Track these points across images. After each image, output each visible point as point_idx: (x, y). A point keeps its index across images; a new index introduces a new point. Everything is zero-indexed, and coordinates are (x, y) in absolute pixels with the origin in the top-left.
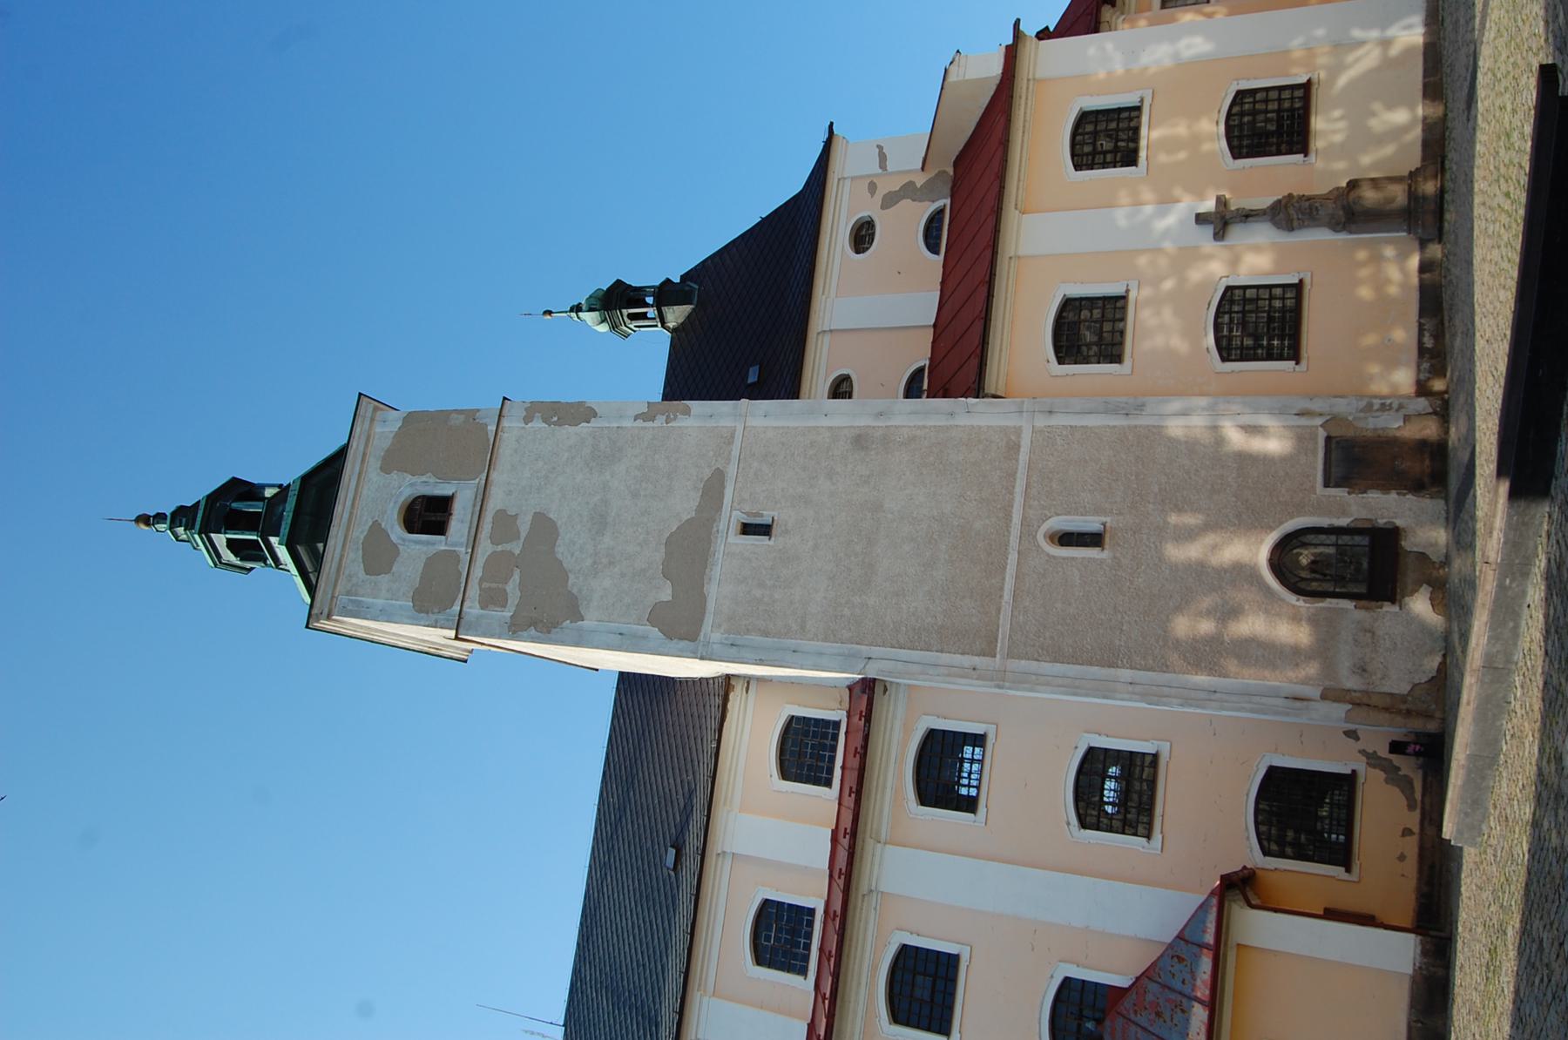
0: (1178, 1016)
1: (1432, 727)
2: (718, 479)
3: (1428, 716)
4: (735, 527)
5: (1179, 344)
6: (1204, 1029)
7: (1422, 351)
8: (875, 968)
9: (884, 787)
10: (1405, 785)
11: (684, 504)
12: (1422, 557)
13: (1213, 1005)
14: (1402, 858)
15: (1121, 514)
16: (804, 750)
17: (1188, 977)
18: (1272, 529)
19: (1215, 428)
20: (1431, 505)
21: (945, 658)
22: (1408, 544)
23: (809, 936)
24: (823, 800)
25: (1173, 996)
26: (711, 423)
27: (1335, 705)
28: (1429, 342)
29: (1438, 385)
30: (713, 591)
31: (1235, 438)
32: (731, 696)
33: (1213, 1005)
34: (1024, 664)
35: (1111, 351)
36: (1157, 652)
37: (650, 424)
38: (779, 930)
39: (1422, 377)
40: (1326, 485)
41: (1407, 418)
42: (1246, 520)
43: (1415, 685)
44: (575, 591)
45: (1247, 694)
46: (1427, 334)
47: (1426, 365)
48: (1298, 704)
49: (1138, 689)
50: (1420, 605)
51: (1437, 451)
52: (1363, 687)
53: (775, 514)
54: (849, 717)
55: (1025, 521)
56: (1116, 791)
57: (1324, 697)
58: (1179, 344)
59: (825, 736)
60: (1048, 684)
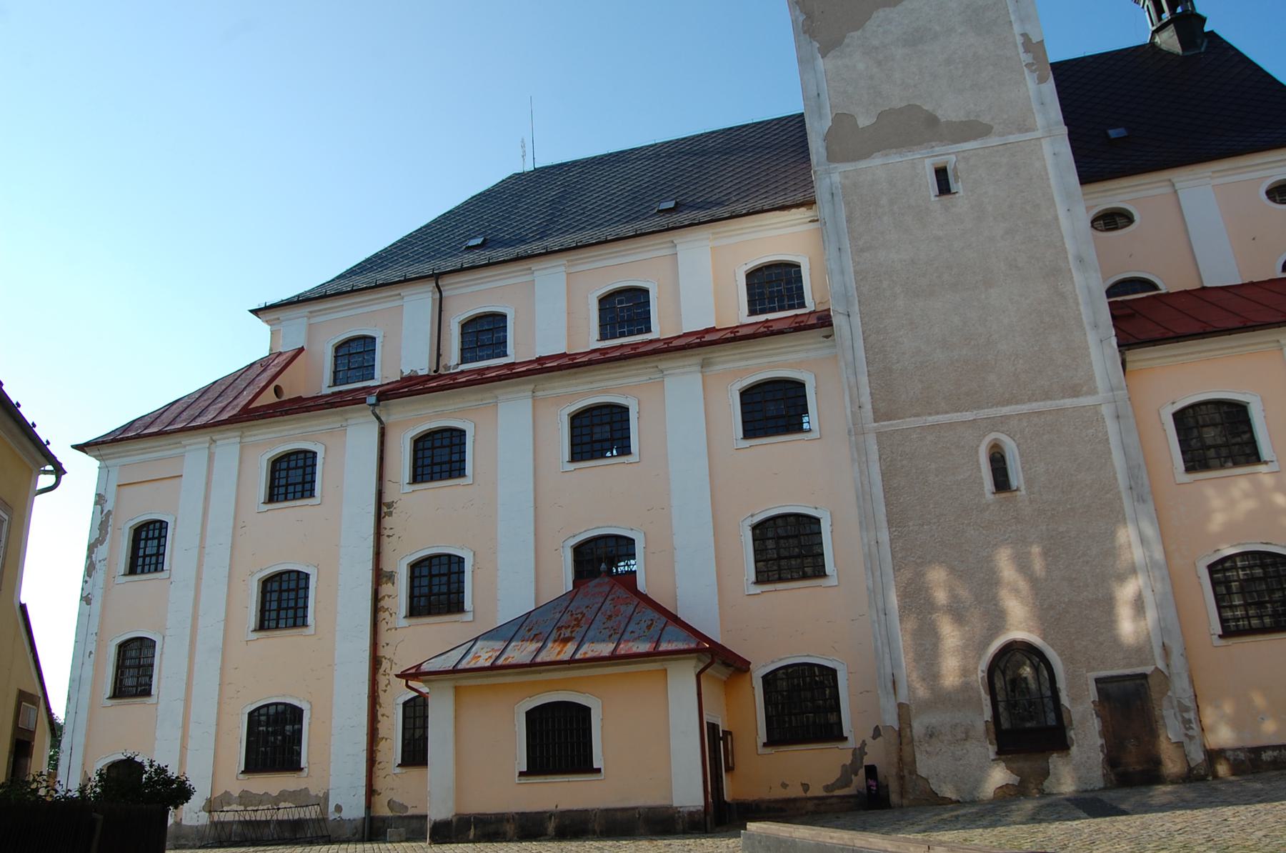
0: (607, 632)
1: (894, 798)
2: (985, 131)
3: (902, 794)
4: (940, 161)
5: (1218, 521)
6: (595, 654)
7: (1257, 751)
8: (605, 391)
9: (747, 359)
10: (844, 781)
11: (950, 109)
12: (1046, 773)
13: (614, 658)
14: (784, 786)
15: (1031, 502)
16: (773, 285)
17: (636, 635)
18: (1044, 639)
19: (1133, 570)
20: (1097, 776)
21: (864, 379)
22: (1055, 761)
23: (631, 334)
24: (738, 313)
25: (623, 626)
26: (1035, 106)
27: (896, 717)
28: (1266, 756)
29: (1222, 769)
30: (876, 161)
31: (1127, 591)
32: (802, 209)
33: (614, 658)
34: (873, 448)
35: (1196, 460)
36: (909, 558)
37: (1021, 50)
38: (629, 309)
39: (1229, 754)
40: (1098, 681)
41: (1180, 745)
42: (1046, 614)
43: (927, 780)
44: (846, 41)
45: (889, 641)
46: (1275, 754)
47: (1242, 756)
48: (890, 685)
49: (874, 549)
50: (998, 776)
51: (1151, 775)
52: (916, 738)
53: (961, 193)
54: (810, 313)
55: (1006, 418)
56: (788, 548)
57: (900, 706)
58: (1218, 521)
59: (791, 298)
60: (861, 472)
